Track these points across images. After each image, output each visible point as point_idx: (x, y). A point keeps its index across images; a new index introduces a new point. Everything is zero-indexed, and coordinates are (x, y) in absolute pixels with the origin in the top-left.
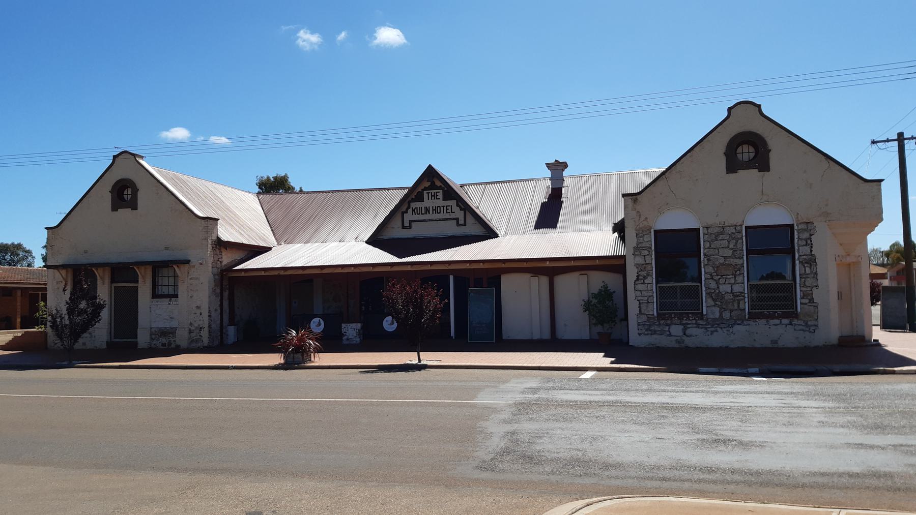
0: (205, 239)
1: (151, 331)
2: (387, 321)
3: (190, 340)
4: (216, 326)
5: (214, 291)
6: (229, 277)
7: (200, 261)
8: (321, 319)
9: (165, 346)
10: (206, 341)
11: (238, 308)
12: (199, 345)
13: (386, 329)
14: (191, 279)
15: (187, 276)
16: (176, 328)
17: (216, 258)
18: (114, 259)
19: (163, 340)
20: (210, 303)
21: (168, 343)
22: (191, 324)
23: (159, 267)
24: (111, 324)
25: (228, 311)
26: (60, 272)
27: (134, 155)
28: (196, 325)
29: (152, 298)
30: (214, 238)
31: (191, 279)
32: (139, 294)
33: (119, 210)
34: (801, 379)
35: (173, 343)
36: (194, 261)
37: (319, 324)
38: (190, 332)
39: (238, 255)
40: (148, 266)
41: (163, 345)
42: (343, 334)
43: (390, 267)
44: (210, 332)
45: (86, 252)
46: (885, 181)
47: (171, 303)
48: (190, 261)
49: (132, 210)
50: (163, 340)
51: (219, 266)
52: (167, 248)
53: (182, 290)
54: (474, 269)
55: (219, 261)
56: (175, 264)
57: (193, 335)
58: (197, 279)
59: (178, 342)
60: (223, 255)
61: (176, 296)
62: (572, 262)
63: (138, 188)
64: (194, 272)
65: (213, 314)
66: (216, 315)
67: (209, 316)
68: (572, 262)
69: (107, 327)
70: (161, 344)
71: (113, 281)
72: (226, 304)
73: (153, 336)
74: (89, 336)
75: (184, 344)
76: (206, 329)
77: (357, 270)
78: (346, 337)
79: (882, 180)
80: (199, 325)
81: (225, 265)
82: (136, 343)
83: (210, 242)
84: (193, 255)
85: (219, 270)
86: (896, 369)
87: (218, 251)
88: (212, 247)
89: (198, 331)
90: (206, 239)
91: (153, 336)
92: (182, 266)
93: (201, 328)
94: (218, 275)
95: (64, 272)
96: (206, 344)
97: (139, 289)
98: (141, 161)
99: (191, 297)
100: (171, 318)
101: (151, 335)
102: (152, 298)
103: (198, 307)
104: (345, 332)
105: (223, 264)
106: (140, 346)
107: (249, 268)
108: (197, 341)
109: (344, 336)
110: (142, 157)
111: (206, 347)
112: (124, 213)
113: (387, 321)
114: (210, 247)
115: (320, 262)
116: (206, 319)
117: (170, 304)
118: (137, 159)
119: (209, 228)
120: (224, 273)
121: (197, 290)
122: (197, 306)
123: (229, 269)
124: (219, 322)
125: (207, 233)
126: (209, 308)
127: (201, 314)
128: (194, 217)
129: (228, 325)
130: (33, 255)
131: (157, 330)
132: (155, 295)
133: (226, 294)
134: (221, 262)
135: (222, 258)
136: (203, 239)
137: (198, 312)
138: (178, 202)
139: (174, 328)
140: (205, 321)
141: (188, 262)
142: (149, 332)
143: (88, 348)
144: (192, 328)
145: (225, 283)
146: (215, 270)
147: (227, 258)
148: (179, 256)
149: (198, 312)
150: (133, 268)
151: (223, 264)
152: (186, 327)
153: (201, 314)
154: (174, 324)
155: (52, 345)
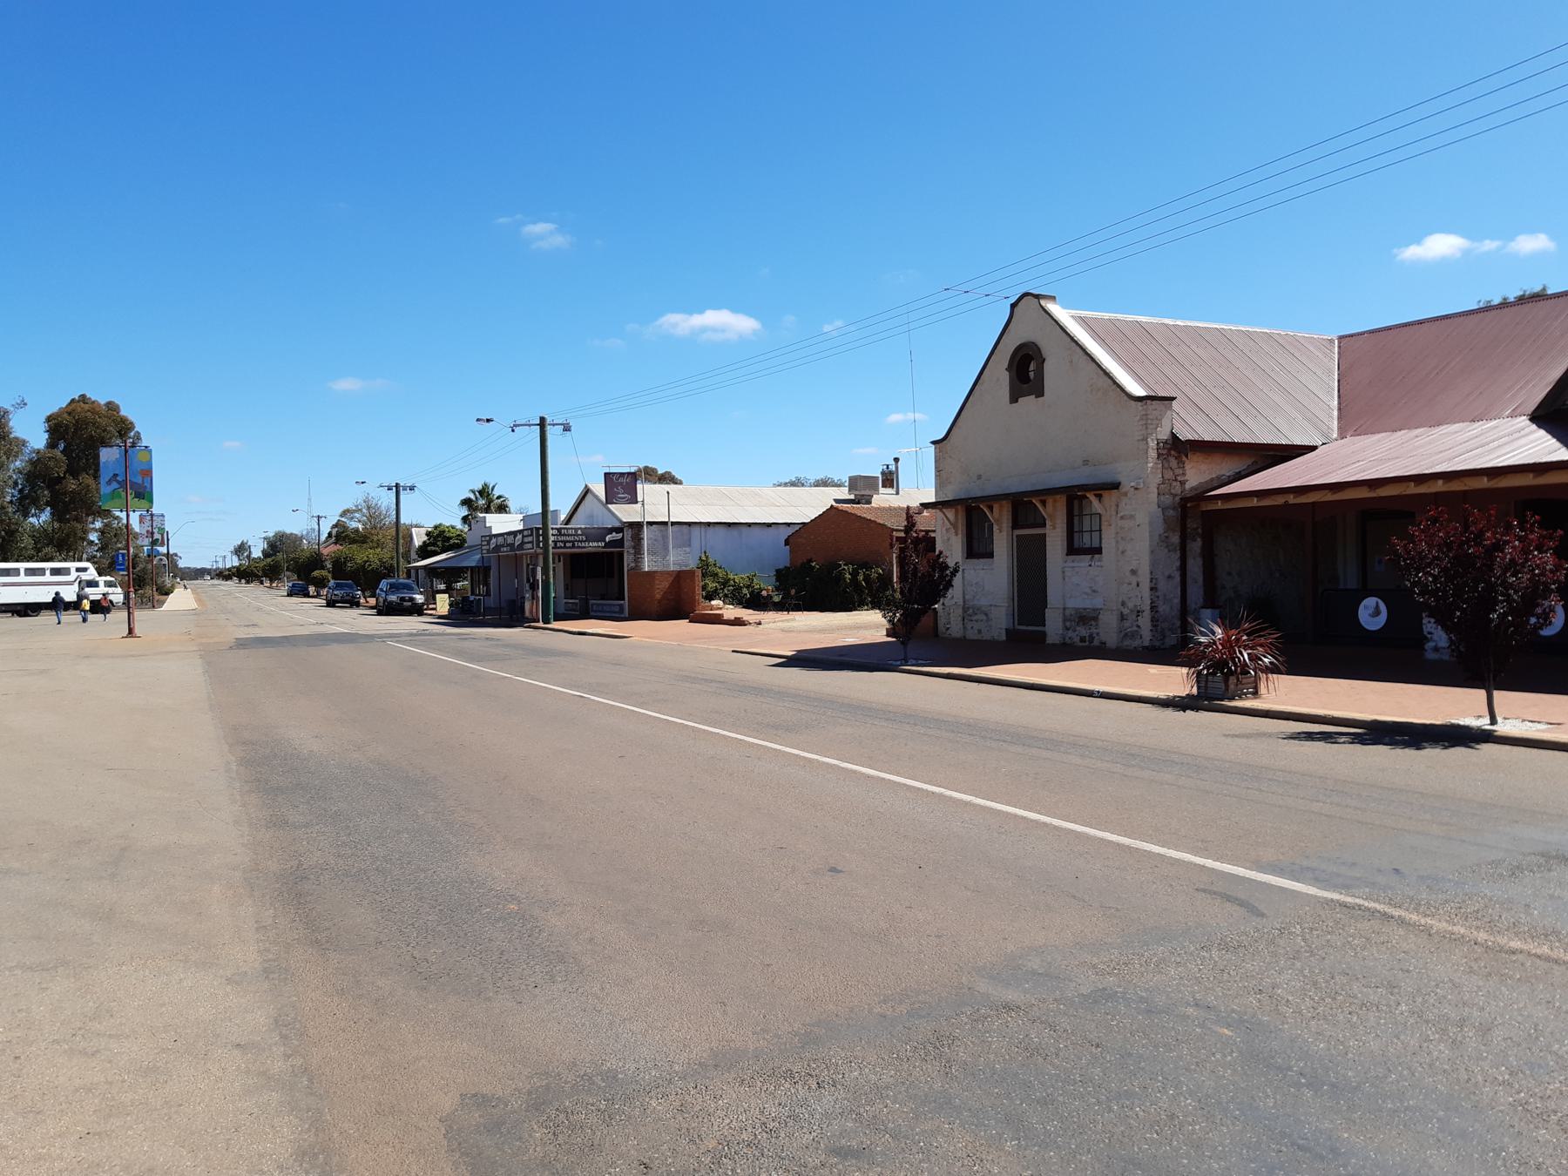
0: (1143, 440)
1: (1064, 615)
2: (1366, 607)
3: (1123, 634)
4: (1169, 608)
5: (1164, 540)
6: (1203, 511)
7: (1133, 484)
8: (1380, 601)
9: (1085, 642)
10: (1146, 636)
11: (1229, 574)
12: (1137, 643)
13: (1363, 624)
14: (1122, 518)
15: (1114, 513)
16: (1101, 609)
17: (1168, 475)
18: (1015, 486)
19: (1083, 631)
20: (1154, 564)
21: (1089, 636)
22: (1123, 604)
23: (1076, 497)
24: (1013, 599)
25: (1201, 579)
26: (944, 513)
27: (1038, 297)
28: (1131, 605)
29: (1067, 555)
30: (1164, 434)
31: (1122, 518)
32: (1047, 548)
33: (1020, 400)
34: (1345, 717)
35: (1097, 638)
36: (1127, 485)
37: (1377, 612)
38: (1122, 618)
39: (1226, 467)
40: (1058, 497)
41: (1083, 640)
42: (1426, 638)
43: (1531, 475)
44: (1153, 620)
45: (979, 477)
46: (932, 440)
47: (1093, 564)
48: (1120, 484)
49: (1036, 397)
50: (1083, 631)
51: (1177, 489)
52: (1086, 462)
53: (1108, 543)
54: (1313, 503)
55: (1176, 480)
56: (982, 502)
57: (1127, 624)
58: (1132, 517)
59: (1103, 638)
60: (1186, 468)
61: (1099, 551)
62: (1219, 502)
63: (1044, 356)
64: (1126, 504)
65: (1162, 585)
66: (1172, 589)
67: (1152, 589)
68: (1486, 479)
69: (1006, 605)
70: (1079, 638)
71: (1016, 525)
72: (1195, 566)
73: (1068, 624)
74: (985, 618)
75: (1112, 639)
76: (1147, 614)
77: (1456, 486)
78: (1431, 644)
79: (1174, 399)
80: (1136, 606)
81: (1192, 489)
82: (1044, 634)
83: (1153, 444)
84: (1123, 472)
85: (1177, 498)
86: (532, 624)
87: (1174, 463)
88: (1159, 455)
89: (1134, 617)
90: (1145, 439)
91: (1068, 624)
92: (1106, 494)
93: (1138, 612)
94: (1174, 509)
95: (950, 514)
96: (1147, 643)
97: (1047, 539)
98: (1052, 307)
99: (1123, 552)
100: (1094, 591)
101: (1065, 621)
102: (1067, 555)
103: (1134, 572)
104: (1430, 633)
105: (1188, 486)
106: (1049, 640)
107: (1554, 459)
108: (1133, 635)
109: (1429, 641)
110: (1053, 298)
111: (1147, 648)
112: (1028, 402)
113: (1366, 607)
114: (1153, 454)
115: (1484, 460)
116: (1146, 594)
117: (1090, 565)
118: (1043, 302)
119: (1149, 417)
120: (1189, 505)
121: (1132, 539)
122: (1132, 570)
123: (1200, 496)
124: (1177, 601)
125: (1147, 428)
126: (1151, 573)
127: (1138, 585)
128: (1125, 398)
129: (1202, 608)
130: (54, 596)
131: (1073, 613)
132: (1072, 550)
133: (1196, 546)
134: (1183, 483)
135: (1184, 474)
136: (1139, 440)
137: (1134, 580)
138: (1101, 372)
139: (1097, 609)
140: (1143, 598)
141: (1115, 486)
142: (1061, 615)
143: (984, 638)
144: (1126, 611)
145: (1192, 524)
146: (1167, 500)
147: (1196, 474)
148: (1101, 476)
149: (1134, 580)
150: (1031, 502)
151: (1188, 486)
152: (1115, 608)
153: (1138, 585)
154: (1097, 602)
155: (944, 631)
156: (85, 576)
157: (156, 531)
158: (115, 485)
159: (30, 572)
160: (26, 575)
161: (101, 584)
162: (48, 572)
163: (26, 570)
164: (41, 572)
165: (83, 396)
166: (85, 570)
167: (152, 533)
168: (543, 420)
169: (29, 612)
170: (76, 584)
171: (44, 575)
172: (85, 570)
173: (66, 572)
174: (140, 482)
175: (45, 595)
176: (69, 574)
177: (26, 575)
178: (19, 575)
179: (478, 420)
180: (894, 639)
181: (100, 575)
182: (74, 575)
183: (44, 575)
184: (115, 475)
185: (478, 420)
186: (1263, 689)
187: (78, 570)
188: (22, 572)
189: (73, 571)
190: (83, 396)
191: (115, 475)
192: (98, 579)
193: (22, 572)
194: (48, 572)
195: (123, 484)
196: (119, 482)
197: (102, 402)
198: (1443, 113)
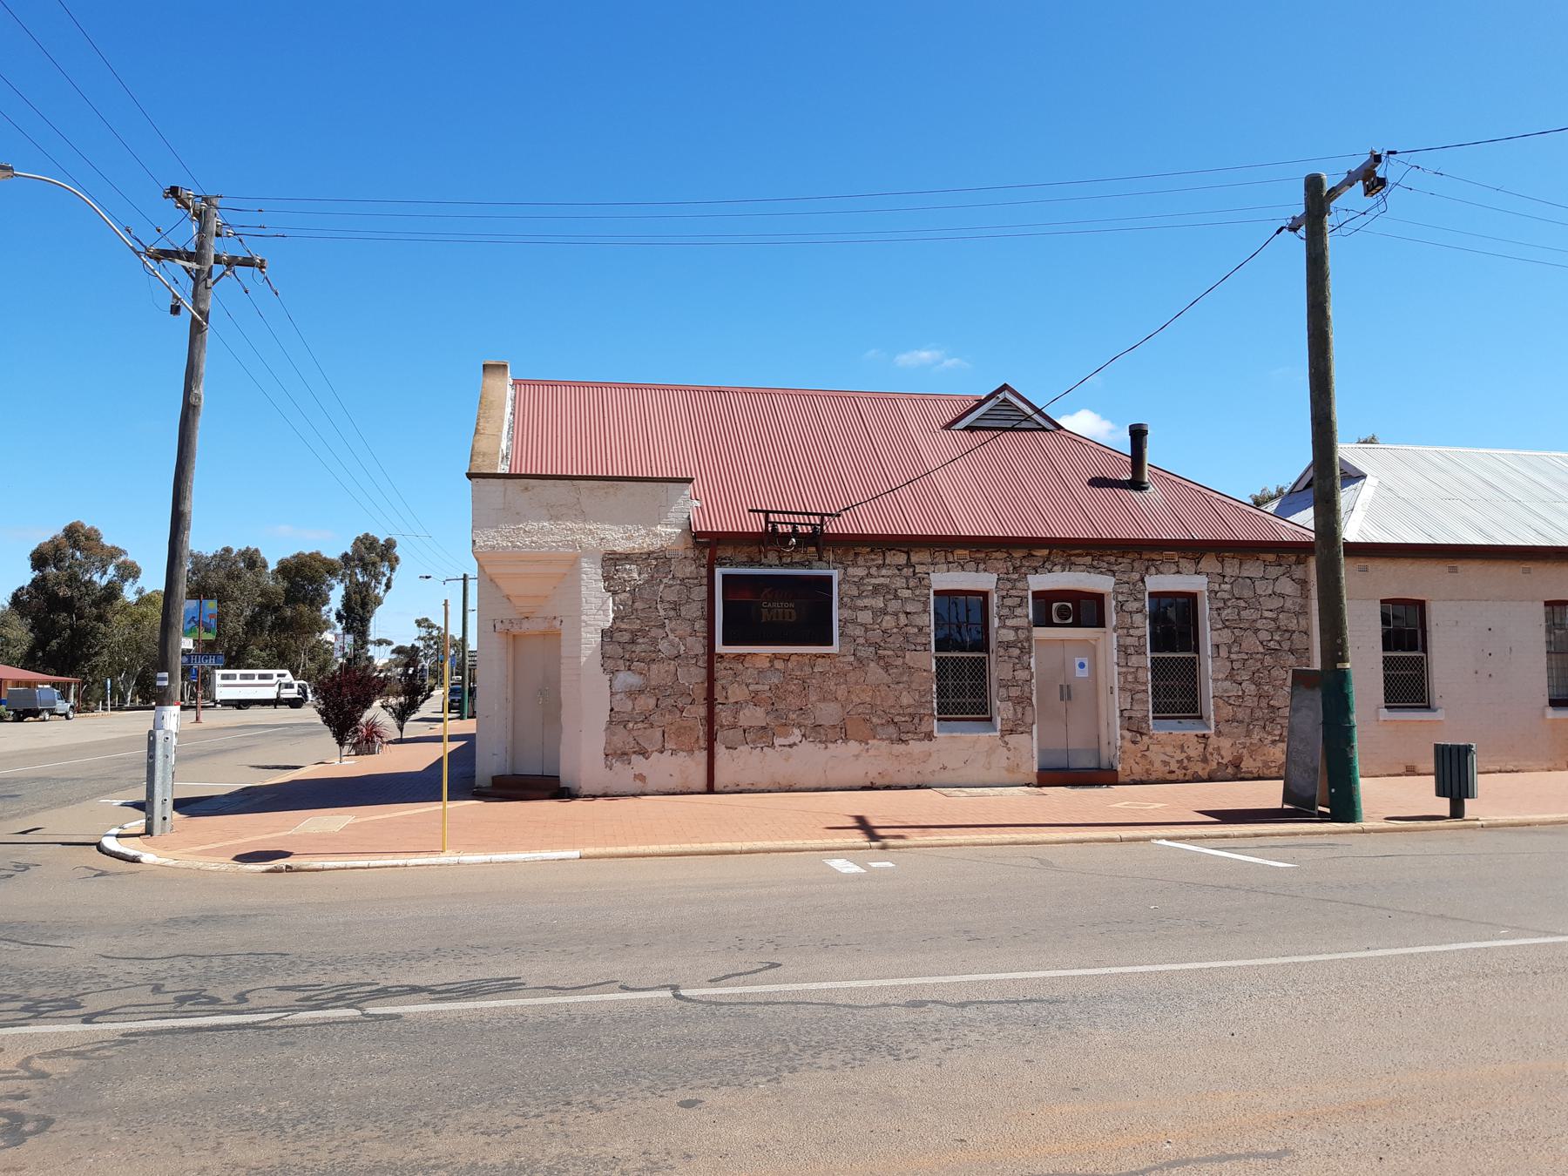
156: (284, 680)
157: (346, 646)
158: (193, 624)
159: (244, 677)
160: (241, 679)
161: (296, 686)
162: (257, 677)
163: (241, 675)
164: (252, 677)
165: (367, 535)
166: (284, 675)
167: (344, 648)
168: (465, 575)
169: (242, 706)
170: (277, 686)
171: (254, 679)
172: (284, 675)
173: (269, 677)
174: (208, 621)
175: (270, 693)
176: (272, 678)
177: (241, 679)
178: (235, 679)
179: (421, 577)
180: (464, 742)
181: (295, 680)
182: (276, 679)
183: (254, 679)
184: (193, 618)
185: (421, 577)
186: (491, 781)
187: (279, 675)
188: (238, 676)
189: (275, 676)
190: (367, 535)
191: (193, 618)
192: (293, 682)
193: (238, 676)
194: (257, 677)
195: (198, 624)
196: (195, 622)
197: (262, 556)
198: (1414, 242)
